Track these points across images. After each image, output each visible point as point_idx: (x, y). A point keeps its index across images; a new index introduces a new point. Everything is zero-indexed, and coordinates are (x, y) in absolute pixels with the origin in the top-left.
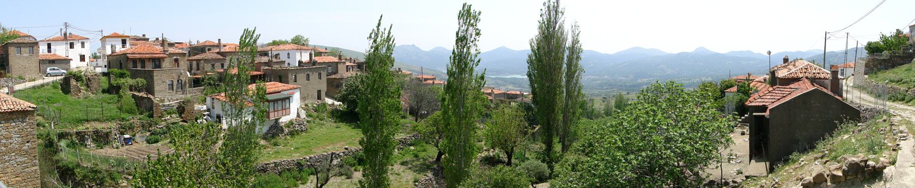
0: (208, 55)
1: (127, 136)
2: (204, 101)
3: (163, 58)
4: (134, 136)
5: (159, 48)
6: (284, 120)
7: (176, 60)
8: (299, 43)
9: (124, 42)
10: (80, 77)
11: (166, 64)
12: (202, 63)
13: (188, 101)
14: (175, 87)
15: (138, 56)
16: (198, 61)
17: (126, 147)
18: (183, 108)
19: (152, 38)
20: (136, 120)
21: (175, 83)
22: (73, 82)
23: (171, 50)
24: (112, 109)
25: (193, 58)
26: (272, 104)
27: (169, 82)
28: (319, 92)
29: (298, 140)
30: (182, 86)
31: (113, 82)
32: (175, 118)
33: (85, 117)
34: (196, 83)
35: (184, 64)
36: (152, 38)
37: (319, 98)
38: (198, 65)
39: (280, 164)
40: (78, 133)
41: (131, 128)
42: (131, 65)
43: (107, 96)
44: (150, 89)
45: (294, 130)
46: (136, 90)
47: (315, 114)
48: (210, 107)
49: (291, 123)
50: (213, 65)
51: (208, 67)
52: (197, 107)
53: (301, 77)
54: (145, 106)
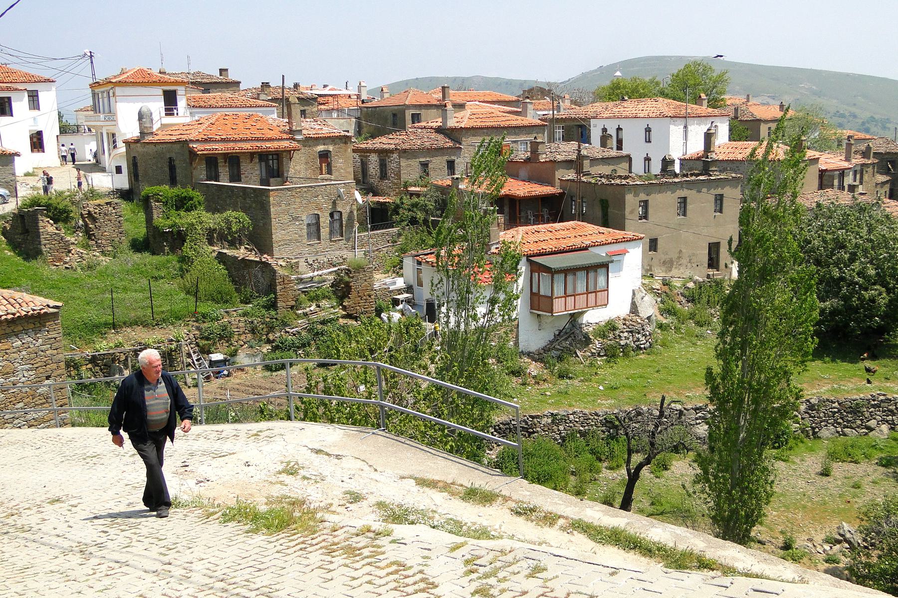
0: (412, 137)
1: (217, 357)
2: (397, 269)
3: (289, 152)
4: (234, 354)
5: (273, 117)
6: (593, 318)
7: (325, 156)
8: (694, 86)
9: (170, 100)
10: (65, 211)
11: (298, 167)
12: (393, 161)
13: (359, 269)
14: (325, 232)
15: (220, 148)
16: (384, 154)
17: (216, 383)
18: (347, 285)
19: (250, 82)
20: (234, 316)
21: (325, 220)
22: (47, 227)
23: (309, 127)
24: (171, 292)
25: (370, 144)
26: (559, 279)
27: (306, 219)
28: (714, 248)
29: (621, 370)
30: (340, 226)
31: (159, 219)
32: (329, 309)
33: (110, 319)
34: (379, 217)
35: (345, 164)
36: (250, 82)
37: (713, 263)
38: (383, 166)
39: (564, 419)
40: (93, 360)
41: (225, 336)
42: (200, 172)
43: (146, 258)
44: (260, 239)
45: (616, 344)
46: (222, 237)
47: (687, 308)
48: (413, 281)
49: (611, 326)
50: (425, 165)
51: (410, 170)
52: (382, 280)
53: (663, 204)
54: (254, 282)
